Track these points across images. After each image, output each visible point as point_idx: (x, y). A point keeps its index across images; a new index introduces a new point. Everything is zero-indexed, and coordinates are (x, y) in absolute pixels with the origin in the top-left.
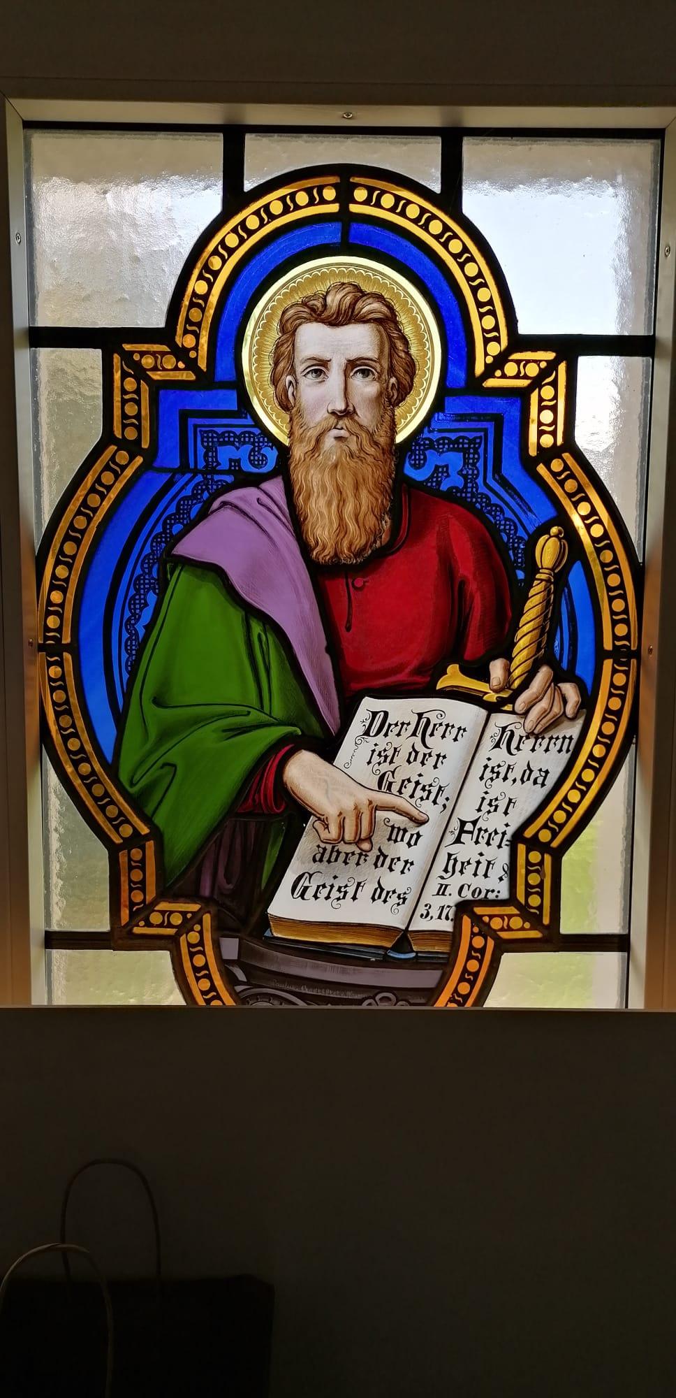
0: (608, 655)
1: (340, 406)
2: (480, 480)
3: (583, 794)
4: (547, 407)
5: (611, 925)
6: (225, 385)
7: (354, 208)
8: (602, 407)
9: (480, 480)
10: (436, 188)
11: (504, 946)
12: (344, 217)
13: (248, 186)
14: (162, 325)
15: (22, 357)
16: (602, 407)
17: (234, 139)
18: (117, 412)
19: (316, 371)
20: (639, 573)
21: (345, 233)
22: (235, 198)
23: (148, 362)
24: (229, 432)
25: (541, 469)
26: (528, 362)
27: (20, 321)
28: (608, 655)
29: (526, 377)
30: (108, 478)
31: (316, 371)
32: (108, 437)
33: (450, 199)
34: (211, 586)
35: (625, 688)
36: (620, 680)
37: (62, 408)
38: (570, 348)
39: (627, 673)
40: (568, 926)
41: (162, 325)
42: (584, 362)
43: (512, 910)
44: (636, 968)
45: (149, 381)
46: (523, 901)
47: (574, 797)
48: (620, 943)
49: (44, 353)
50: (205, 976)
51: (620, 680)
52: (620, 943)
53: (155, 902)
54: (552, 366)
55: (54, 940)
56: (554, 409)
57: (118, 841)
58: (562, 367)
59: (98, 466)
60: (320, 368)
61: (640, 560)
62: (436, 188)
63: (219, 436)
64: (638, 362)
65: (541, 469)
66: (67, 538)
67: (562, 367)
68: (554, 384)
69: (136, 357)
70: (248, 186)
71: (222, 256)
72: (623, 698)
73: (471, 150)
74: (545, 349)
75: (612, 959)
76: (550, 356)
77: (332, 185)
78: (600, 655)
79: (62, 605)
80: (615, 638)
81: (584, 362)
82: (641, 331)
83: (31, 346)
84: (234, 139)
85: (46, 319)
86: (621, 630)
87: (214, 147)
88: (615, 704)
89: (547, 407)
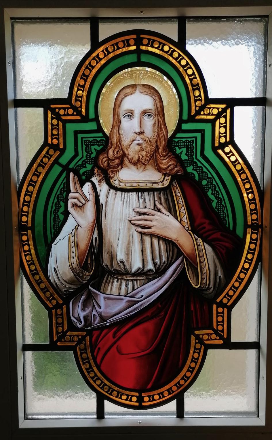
0: (30, 228)
1: (138, 130)
2: (194, 156)
3: (240, 283)
4: (60, 324)
5: (252, 338)
6: (92, 120)
7: (137, 394)
8: (246, 126)
9: (194, 156)
10: (176, 40)
11: (208, 347)
12: (138, 52)
13: (100, 40)
14: (209, 350)
15: (11, 111)
16: (246, 126)
17: (95, 23)
18: (50, 133)
19: (128, 116)
20: (261, 194)
21: (139, 58)
22: (95, 44)
23: (62, 112)
24: (95, 140)
25: (220, 151)
26: (214, 108)
27: (10, 96)
28: (30, 228)
29: (213, 114)
30: (231, 293)
31: (128, 116)
32: (230, 309)
33: (181, 44)
34: (187, 252)
35: (256, 240)
36: (254, 236)
37: (28, 132)
38: (231, 103)
39: (257, 234)
40: (234, 339)
41: (209, 350)
42: (237, 109)
43: (64, 118)
44: (263, 355)
45: (213, 329)
46: (60, 122)
47: (237, 284)
48: (255, 346)
49: (20, 110)
50: (87, 362)
51: (254, 236)
52: (255, 346)
53: (67, 331)
54: (224, 110)
55: (26, 348)
56: (225, 127)
57: (51, 306)
58: (228, 111)
59: (234, 298)
60: (130, 114)
61: (262, 188)
62: (176, 40)
63: (91, 142)
64: (260, 108)
65: (220, 151)
66: (247, 270)
67: (228, 111)
68: (225, 117)
69: (218, 338)
70: (100, 40)
71: (90, 69)
72: (256, 244)
73: (190, 27)
74: (108, 277)
75: (252, 353)
76: (223, 106)
77: (134, 39)
78: (246, 226)
79: (27, 212)
80: (252, 220)
81: (237, 109)
82: (261, 96)
83: (15, 107)
84: (95, 23)
85: (21, 96)
86: (254, 217)
87: (86, 28)
88: (253, 246)
89: (60, 324)
